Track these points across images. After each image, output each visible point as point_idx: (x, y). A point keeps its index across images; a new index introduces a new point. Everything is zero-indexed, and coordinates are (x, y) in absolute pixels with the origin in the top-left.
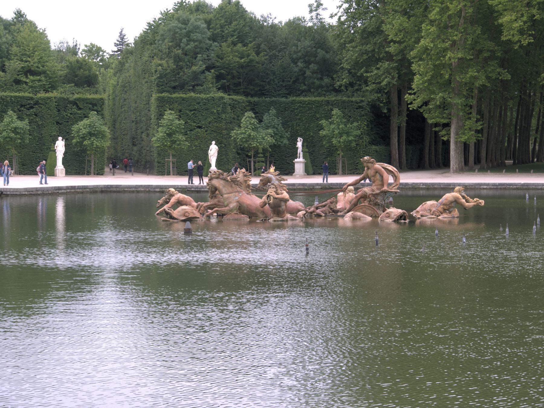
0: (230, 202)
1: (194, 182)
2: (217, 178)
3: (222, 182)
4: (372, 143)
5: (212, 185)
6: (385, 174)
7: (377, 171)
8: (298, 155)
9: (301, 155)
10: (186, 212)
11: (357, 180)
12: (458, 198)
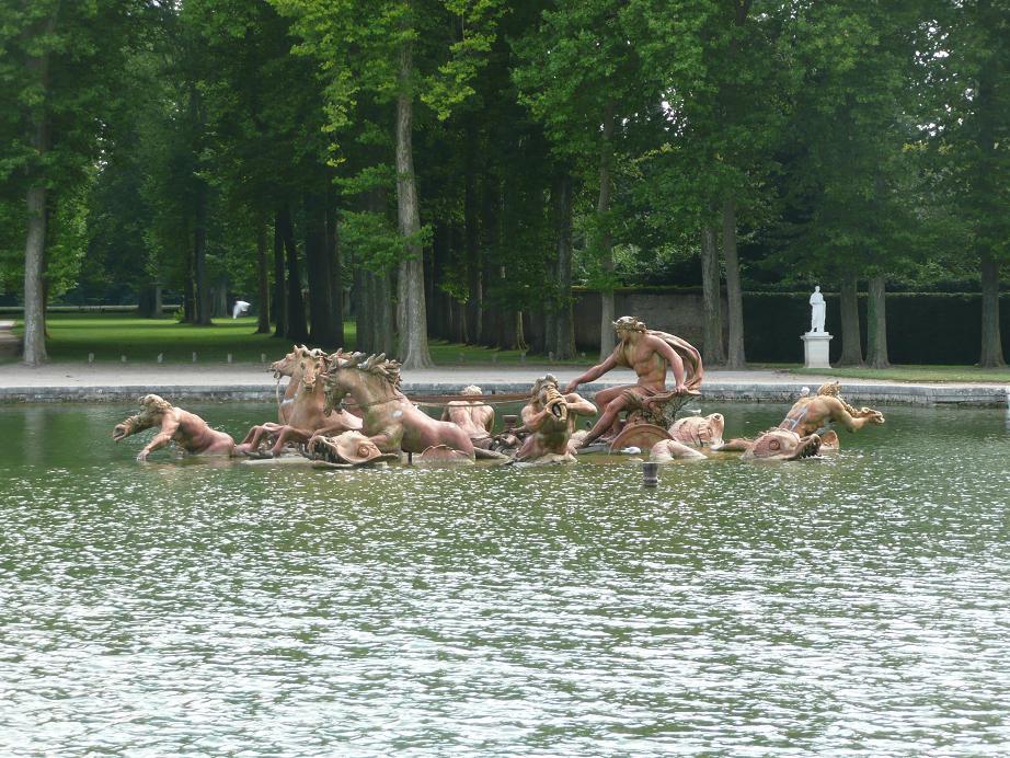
0: (387, 424)
3: (362, 377)
6: (678, 358)
7: (656, 349)
10: (363, 446)
12: (838, 408)
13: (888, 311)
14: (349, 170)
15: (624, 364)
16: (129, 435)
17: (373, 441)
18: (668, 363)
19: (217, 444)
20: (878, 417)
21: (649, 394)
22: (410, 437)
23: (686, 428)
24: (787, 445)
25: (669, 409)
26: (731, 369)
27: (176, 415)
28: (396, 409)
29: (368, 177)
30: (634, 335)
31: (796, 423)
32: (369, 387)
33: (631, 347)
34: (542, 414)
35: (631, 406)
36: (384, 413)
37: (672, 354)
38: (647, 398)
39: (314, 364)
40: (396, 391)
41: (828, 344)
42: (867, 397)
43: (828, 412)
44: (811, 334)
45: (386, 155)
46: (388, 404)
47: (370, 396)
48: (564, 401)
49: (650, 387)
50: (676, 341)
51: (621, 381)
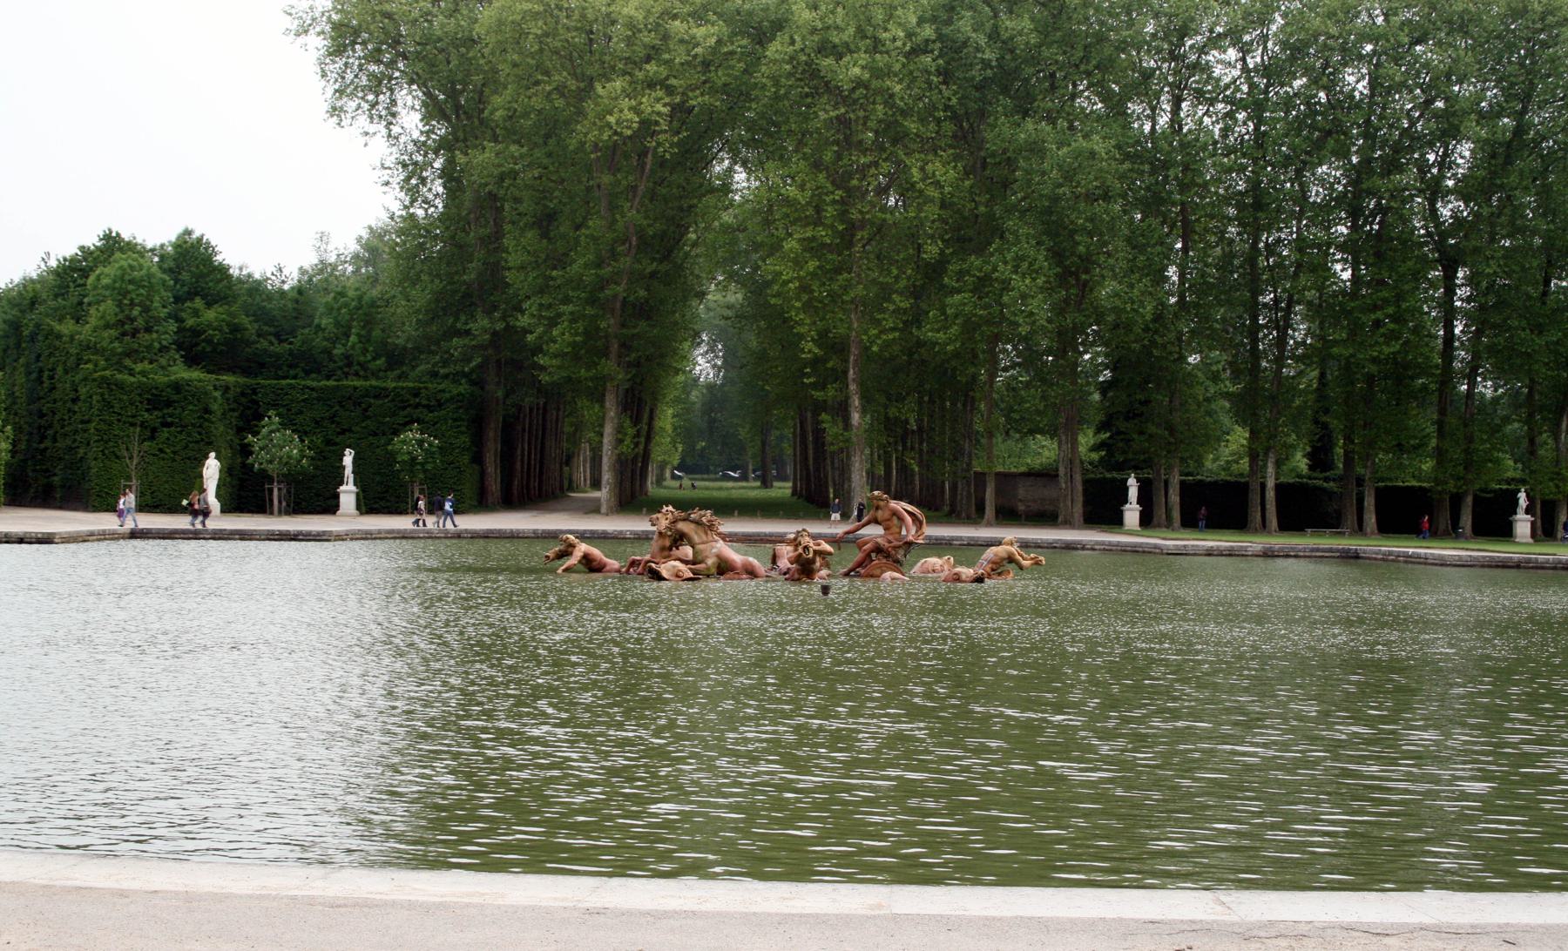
3: (693, 526)
6: (909, 519)
7: (895, 513)
13: (1085, 491)
15: (876, 521)
18: (901, 519)
25: (901, 552)
27: (582, 548)
29: (831, 392)
35: (878, 550)
44: (342, 488)
47: (696, 539)
50: (910, 508)
51: (873, 532)
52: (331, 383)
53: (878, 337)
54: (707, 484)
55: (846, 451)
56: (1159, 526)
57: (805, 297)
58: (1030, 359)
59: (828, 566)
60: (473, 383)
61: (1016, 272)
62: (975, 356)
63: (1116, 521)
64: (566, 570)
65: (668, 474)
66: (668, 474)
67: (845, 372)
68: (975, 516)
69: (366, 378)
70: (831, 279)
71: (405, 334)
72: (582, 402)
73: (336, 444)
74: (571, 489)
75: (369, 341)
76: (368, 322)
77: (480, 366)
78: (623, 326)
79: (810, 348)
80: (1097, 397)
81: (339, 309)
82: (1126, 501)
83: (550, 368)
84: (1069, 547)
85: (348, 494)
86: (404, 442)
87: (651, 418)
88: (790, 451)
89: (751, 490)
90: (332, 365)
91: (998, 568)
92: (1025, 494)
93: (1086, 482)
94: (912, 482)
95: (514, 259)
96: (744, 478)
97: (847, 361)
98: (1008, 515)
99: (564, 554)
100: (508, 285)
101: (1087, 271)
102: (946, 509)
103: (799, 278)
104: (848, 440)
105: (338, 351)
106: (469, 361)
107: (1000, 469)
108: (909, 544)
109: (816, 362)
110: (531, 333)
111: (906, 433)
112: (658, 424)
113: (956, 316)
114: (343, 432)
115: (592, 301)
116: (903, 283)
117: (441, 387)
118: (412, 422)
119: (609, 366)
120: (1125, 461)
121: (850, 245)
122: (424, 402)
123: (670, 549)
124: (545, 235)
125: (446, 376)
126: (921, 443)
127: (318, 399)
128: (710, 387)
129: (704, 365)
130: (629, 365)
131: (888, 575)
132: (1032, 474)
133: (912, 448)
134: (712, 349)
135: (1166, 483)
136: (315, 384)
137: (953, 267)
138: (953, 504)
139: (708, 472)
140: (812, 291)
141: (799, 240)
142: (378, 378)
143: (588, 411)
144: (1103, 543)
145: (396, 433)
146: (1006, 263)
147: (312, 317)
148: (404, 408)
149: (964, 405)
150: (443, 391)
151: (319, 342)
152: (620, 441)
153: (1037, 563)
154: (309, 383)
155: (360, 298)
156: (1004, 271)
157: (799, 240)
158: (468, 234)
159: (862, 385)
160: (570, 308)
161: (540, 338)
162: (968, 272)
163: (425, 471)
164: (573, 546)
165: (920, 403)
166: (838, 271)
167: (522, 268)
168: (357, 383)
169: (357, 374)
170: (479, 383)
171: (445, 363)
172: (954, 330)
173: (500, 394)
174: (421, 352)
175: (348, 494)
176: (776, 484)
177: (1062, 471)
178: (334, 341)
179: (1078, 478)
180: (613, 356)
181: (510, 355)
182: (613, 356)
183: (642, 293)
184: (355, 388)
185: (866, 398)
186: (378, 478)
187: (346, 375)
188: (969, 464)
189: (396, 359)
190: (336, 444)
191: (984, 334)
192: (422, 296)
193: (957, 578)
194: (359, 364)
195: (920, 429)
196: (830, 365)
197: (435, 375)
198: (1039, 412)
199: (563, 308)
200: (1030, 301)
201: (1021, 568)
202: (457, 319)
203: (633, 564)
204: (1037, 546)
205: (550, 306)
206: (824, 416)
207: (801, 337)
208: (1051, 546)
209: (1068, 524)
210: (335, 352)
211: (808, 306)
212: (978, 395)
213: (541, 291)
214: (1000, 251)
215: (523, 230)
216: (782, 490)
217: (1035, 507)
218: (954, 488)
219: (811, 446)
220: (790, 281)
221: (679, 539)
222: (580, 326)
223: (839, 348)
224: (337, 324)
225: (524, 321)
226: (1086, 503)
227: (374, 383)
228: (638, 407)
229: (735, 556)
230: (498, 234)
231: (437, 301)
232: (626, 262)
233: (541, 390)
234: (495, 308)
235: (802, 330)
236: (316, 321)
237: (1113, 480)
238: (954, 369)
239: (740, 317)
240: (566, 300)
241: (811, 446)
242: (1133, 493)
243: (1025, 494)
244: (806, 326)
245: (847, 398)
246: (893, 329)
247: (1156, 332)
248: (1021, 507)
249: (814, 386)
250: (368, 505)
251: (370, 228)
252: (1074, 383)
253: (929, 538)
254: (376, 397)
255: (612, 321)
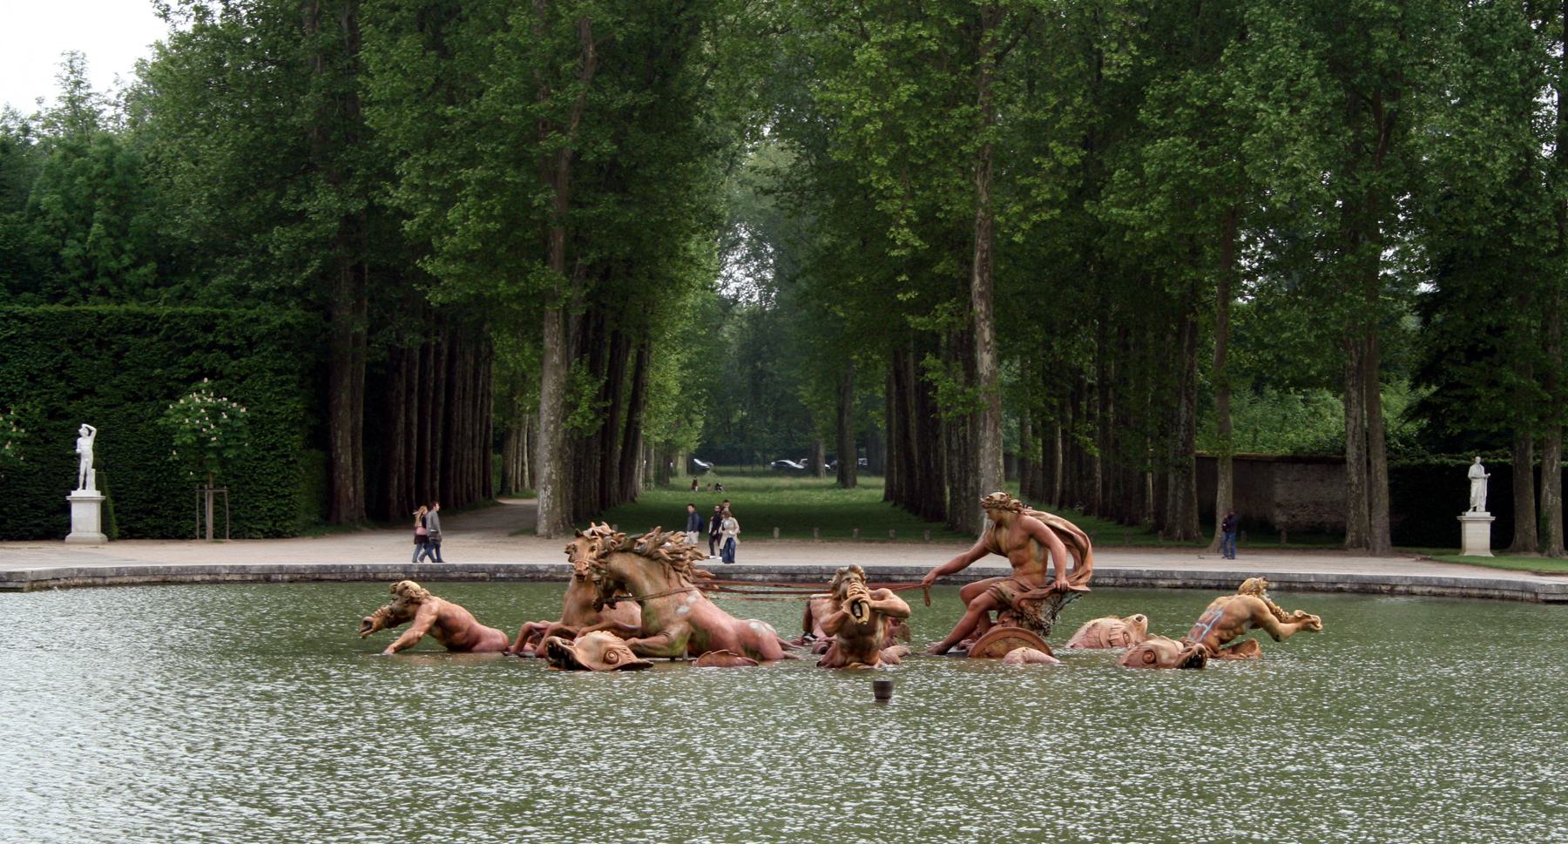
0: (668, 622)
1: (443, 557)
2: (624, 551)
4: (308, 447)
5: (611, 571)
6: (1059, 544)
7: (1033, 534)
8: (81, 479)
9: (91, 479)
10: (611, 650)
11: (964, 558)
13: (1393, 488)
14: (923, 307)
16: (379, 628)
17: (631, 647)
18: (1045, 545)
19: (483, 644)
20: (1314, 623)
21: (1023, 589)
22: (698, 637)
23: (1095, 632)
24: (1164, 657)
25: (1046, 608)
26: (1373, 554)
27: (435, 605)
28: (681, 604)
30: (1008, 515)
31: (1208, 628)
32: (648, 576)
33: (1004, 531)
34: (839, 614)
35: (1002, 604)
36: (666, 608)
37: (1051, 539)
38: (1017, 594)
39: (589, 546)
40: (683, 582)
41: (1488, 527)
42: (1475, 592)
43: (1248, 615)
44: (1469, 514)
45: (959, 289)
46: (671, 598)
47: (648, 587)
48: (866, 597)
49: (1024, 581)
50: (1062, 523)
52: (58, 308)
53: (1023, 217)
54: (747, 481)
55: (971, 420)
56: (1525, 549)
57: (894, 148)
58: (1291, 258)
59: (906, 637)
60: (307, 305)
61: (1266, 98)
62: (1196, 252)
63: (1447, 540)
64: (397, 650)
65: (681, 464)
66: (681, 464)
67: (967, 282)
68: (1197, 536)
69: (120, 300)
70: (940, 116)
71: (188, 221)
72: (503, 342)
73: (65, 416)
74: (505, 491)
75: (125, 233)
76: (123, 201)
77: (323, 275)
78: (575, 202)
79: (905, 239)
80: (1411, 322)
81: (72, 177)
82: (1466, 505)
83: (445, 277)
84: (1367, 589)
85: (86, 506)
86: (185, 411)
87: (640, 367)
88: (881, 425)
89: (820, 491)
90: (59, 277)
91: (1232, 637)
92: (1289, 496)
93: (1393, 473)
94: (1091, 475)
95: (378, 87)
96: (812, 470)
97: (970, 264)
98: (1256, 531)
99: (400, 618)
100: (371, 134)
101: (1395, 95)
102: (1149, 521)
103: (883, 114)
104: (973, 402)
105: (70, 251)
106: (303, 264)
107: (1245, 450)
108: (1062, 593)
109: (917, 264)
110: (411, 217)
111: (1080, 389)
112: (653, 377)
113: (1161, 178)
114: (79, 395)
115: (520, 161)
116: (1066, 121)
117: (252, 314)
118: (199, 377)
119: (549, 276)
120: (1464, 433)
121: (972, 55)
122: (223, 341)
123: (598, 607)
124: (435, 43)
125: (263, 296)
126: (1104, 408)
127: (36, 337)
128: (756, 317)
129: (740, 280)
130: (590, 271)
131: (1018, 653)
132: (1299, 460)
133: (1090, 416)
134: (756, 253)
135: (1538, 471)
136: (27, 310)
137: (1155, 91)
138: (1160, 514)
139: (751, 462)
140: (904, 138)
141: (885, 46)
142: (142, 298)
143: (508, 351)
144: (1427, 582)
145: (173, 396)
146: (1248, 82)
147: (24, 193)
148: (187, 352)
149: (1179, 335)
150: (256, 320)
151: (36, 234)
152: (571, 407)
153: (1308, 628)
154: (18, 308)
155: (109, 160)
156: (1243, 95)
157: (885, 46)
158: (297, 42)
159: (999, 303)
160: (479, 172)
161: (426, 225)
162: (1181, 100)
163: (224, 463)
164: (415, 602)
165: (1102, 337)
166: (951, 101)
167: (394, 102)
168: (103, 308)
169: (104, 292)
170: (325, 309)
171: (260, 271)
172: (1158, 203)
173: (360, 329)
174: (219, 254)
175: (86, 506)
176: (861, 480)
177: (1351, 453)
178: (65, 233)
179: (1381, 465)
180: (556, 256)
181: (375, 255)
182: (556, 256)
183: (607, 147)
184: (100, 317)
185: (1007, 333)
186: (141, 476)
187: (85, 294)
188: (1188, 443)
189: (173, 264)
190: (65, 416)
191: (1213, 211)
192: (218, 155)
193: (1152, 660)
194: (108, 273)
195: (1104, 385)
196: (939, 268)
197: (242, 293)
198: (1310, 350)
199: (465, 173)
200: (1290, 147)
201: (1277, 637)
202: (282, 194)
203: (533, 635)
204: (1309, 587)
205: (444, 169)
206: (929, 360)
207: (888, 219)
208: (1334, 588)
209: (1364, 547)
210: (66, 252)
211: (899, 166)
212: (1203, 319)
213: (429, 144)
214: (1236, 59)
215: (396, 30)
216: (871, 489)
217: (1303, 517)
218: (1162, 484)
219: (914, 414)
220: (868, 119)
221: (616, 587)
222: (496, 204)
223: (956, 239)
224: (69, 204)
225: (398, 196)
226: (1395, 509)
227: (133, 306)
228: (611, 343)
229: (721, 616)
230: (355, 41)
231: (246, 162)
232: (575, 92)
233: (439, 318)
234: (348, 174)
235: (890, 207)
236: (32, 198)
237: (1443, 467)
238: (1161, 273)
239: (789, 189)
240: (471, 159)
241: (914, 414)
242: (1479, 492)
243: (1289, 496)
244: (898, 204)
245: (972, 327)
246: (1051, 204)
247: (1518, 204)
248: (1280, 518)
249: (912, 307)
250: (122, 523)
251: (159, 46)
252: (1372, 297)
253: (1098, 574)
254: (137, 332)
255: (553, 194)
